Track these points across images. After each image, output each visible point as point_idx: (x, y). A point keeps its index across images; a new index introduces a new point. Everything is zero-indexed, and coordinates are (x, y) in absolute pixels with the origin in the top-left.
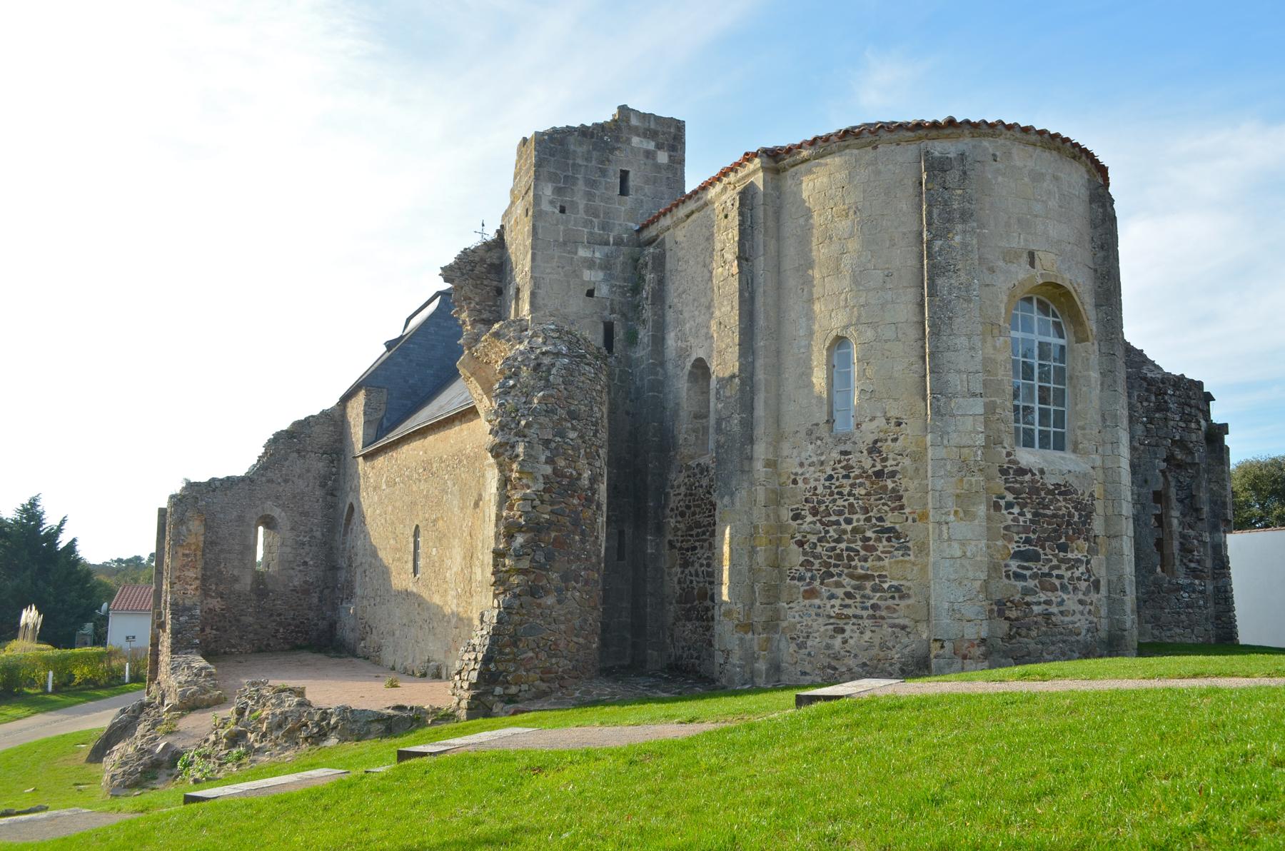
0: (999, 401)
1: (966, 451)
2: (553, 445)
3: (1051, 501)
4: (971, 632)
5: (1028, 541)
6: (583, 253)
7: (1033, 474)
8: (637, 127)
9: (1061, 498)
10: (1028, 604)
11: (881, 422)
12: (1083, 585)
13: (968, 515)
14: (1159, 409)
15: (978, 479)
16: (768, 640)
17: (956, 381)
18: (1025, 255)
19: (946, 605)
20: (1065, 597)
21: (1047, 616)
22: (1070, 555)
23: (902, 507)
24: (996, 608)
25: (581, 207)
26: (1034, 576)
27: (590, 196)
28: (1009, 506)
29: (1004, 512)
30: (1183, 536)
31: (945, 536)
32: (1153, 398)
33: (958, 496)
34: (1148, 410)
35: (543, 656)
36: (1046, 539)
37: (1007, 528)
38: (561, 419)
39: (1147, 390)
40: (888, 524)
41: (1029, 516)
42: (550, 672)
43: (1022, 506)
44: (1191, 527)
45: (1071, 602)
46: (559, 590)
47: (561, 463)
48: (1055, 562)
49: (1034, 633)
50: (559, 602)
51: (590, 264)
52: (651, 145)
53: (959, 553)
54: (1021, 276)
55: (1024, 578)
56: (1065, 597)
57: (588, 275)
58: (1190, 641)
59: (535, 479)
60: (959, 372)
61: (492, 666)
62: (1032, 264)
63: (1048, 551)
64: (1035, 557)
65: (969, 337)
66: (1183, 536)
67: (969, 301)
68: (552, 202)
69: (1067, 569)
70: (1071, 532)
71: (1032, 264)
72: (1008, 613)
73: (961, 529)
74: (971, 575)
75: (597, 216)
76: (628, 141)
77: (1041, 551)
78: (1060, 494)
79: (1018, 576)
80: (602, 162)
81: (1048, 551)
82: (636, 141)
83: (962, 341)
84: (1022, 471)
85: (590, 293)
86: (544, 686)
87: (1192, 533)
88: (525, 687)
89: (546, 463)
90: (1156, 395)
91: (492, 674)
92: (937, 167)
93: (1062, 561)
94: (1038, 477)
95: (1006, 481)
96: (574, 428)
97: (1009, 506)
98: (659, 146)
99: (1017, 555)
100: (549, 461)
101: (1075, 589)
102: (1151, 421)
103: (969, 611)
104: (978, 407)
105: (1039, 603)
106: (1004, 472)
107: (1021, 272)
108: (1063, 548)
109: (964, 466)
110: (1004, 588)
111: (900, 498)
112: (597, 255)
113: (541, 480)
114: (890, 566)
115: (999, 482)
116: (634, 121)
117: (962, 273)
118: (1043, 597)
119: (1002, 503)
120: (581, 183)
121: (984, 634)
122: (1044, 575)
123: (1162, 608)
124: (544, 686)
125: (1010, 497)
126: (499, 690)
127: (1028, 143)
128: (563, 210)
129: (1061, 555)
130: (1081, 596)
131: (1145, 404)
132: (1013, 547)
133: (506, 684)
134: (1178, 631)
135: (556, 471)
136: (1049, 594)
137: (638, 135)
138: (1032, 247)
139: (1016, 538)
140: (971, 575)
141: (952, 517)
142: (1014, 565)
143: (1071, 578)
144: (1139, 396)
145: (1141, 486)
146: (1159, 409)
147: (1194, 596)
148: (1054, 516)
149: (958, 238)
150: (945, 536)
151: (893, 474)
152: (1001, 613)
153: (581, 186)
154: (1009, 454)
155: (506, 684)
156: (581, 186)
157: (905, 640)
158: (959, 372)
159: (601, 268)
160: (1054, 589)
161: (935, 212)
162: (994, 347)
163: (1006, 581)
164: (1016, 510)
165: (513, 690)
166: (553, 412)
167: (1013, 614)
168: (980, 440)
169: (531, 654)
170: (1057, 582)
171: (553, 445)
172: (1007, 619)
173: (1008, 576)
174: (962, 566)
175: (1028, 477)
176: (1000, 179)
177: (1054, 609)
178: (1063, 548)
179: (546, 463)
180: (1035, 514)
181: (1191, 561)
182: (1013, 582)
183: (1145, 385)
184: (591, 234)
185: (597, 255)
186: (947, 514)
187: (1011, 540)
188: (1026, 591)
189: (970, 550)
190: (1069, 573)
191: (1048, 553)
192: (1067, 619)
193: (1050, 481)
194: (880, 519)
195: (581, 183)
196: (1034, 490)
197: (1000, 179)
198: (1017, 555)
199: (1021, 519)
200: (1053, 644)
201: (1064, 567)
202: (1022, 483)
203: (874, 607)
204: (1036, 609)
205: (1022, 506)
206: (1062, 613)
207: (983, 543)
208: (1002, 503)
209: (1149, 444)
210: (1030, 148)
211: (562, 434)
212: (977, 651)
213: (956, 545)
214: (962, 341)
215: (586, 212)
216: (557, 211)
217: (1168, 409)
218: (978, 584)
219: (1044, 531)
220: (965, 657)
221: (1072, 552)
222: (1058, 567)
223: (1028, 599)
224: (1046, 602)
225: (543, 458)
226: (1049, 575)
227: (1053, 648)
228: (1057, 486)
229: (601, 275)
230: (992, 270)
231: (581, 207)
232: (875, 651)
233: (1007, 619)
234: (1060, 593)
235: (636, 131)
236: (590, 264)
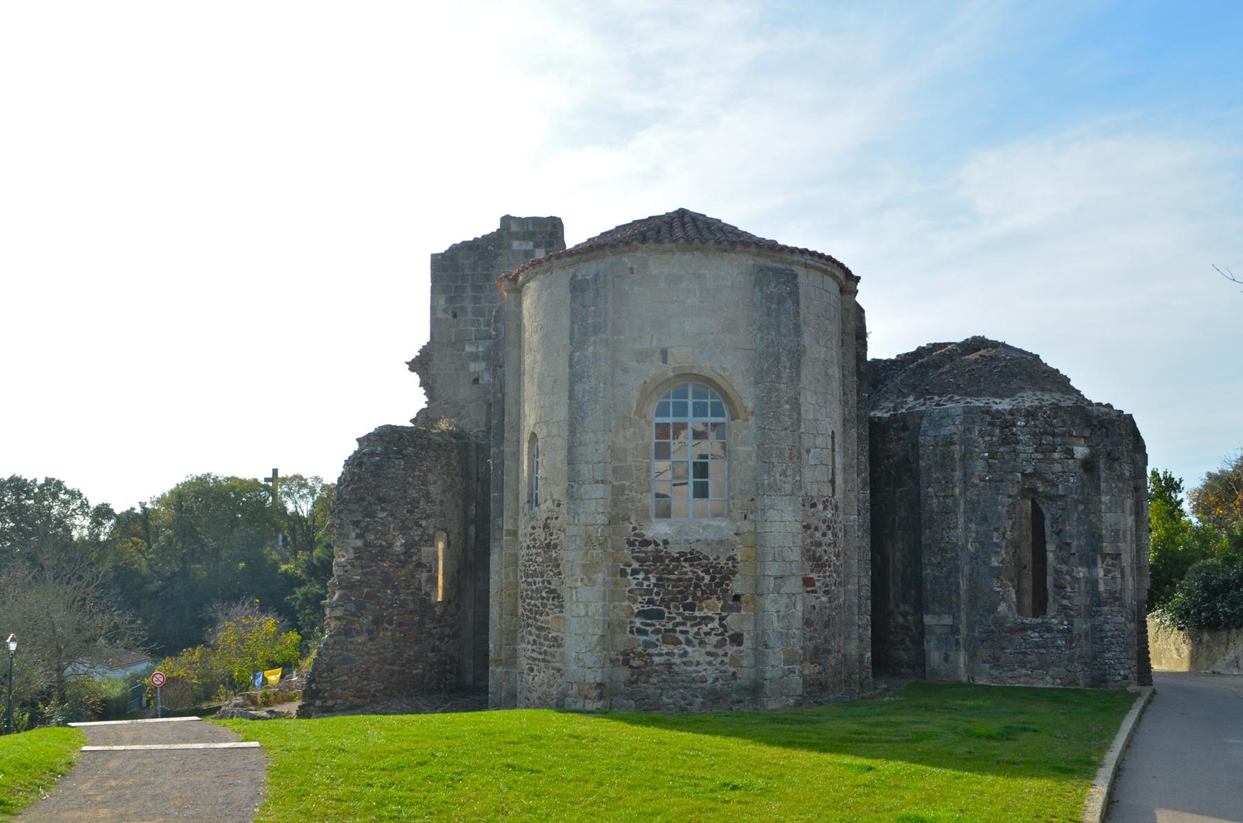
0: (627, 483)
1: (590, 528)
2: (363, 524)
3: (676, 568)
4: (594, 676)
5: (650, 602)
6: (469, 349)
7: (657, 544)
8: (516, 233)
9: (687, 564)
10: (650, 655)
11: (549, 503)
12: (713, 639)
13: (592, 582)
14: (1005, 441)
15: (598, 551)
16: (507, 673)
17: (585, 471)
18: (658, 355)
19: (574, 655)
20: (689, 649)
21: (669, 665)
22: (697, 614)
23: (560, 573)
24: (621, 658)
25: (469, 310)
26: (657, 632)
27: (476, 300)
28: (635, 572)
29: (630, 577)
30: (1056, 571)
31: (574, 598)
32: (997, 431)
33: (584, 566)
34: (991, 444)
35: (356, 679)
36: (671, 600)
37: (630, 591)
38: (370, 504)
39: (990, 424)
40: (553, 587)
41: (653, 580)
42: (362, 691)
43: (647, 572)
44: (1065, 562)
45: (695, 653)
46: (370, 632)
47: (371, 537)
48: (679, 619)
49: (654, 680)
50: (371, 639)
51: (475, 357)
52: (530, 246)
53: (583, 613)
54: (653, 372)
55: (645, 633)
56: (689, 649)
57: (473, 367)
58: (1040, 685)
59: (347, 551)
60: (587, 462)
61: (313, 686)
62: (665, 361)
63: (672, 609)
64: (660, 615)
65: (595, 433)
66: (1056, 571)
67: (596, 402)
68: (445, 311)
69: (692, 626)
70: (699, 594)
71: (665, 361)
72: (632, 663)
73: (586, 593)
74: (591, 631)
75: (482, 315)
76: (509, 246)
77: (666, 610)
78: (685, 561)
79: (640, 632)
80: (487, 269)
81: (672, 609)
82: (516, 245)
83: (590, 437)
84: (646, 543)
85: (476, 381)
86: (357, 701)
87: (1065, 568)
88: (339, 701)
89: (357, 538)
90: (1002, 429)
91: (313, 691)
92: (577, 287)
93: (686, 618)
94: (661, 547)
95: (633, 551)
96: (383, 510)
97: (635, 572)
98: (537, 246)
99: (641, 614)
100: (359, 536)
101: (702, 643)
102: (992, 456)
103: (589, 660)
104: (600, 491)
105: (661, 655)
106: (631, 544)
107: (653, 369)
108: (691, 607)
109: (589, 541)
110: (624, 640)
111: (558, 566)
112: (481, 349)
113: (351, 551)
114: (548, 619)
115: (627, 552)
116: (514, 228)
117: (593, 379)
118: (665, 649)
119: (629, 570)
120: (469, 290)
121: (599, 680)
122: (667, 631)
123: (1002, 649)
124: (357, 701)
125: (636, 565)
126: (318, 703)
127: (664, 252)
128: (455, 316)
129: (687, 613)
130: (709, 648)
131: (987, 439)
132: (636, 608)
133: (324, 699)
134: (1024, 671)
135: (367, 544)
136: (671, 647)
137: (518, 239)
138: (665, 345)
139: (640, 599)
140: (591, 631)
141: (579, 583)
142: (638, 622)
143: (698, 633)
144: (980, 431)
145: (981, 524)
146: (1005, 441)
147: (1047, 635)
148: (679, 580)
149: (591, 349)
150: (574, 598)
151: (555, 546)
152: (626, 663)
153: (469, 292)
154: (634, 529)
155: (324, 699)
156: (469, 292)
157: (559, 680)
158: (587, 462)
159: (483, 359)
160: (677, 642)
161: (576, 327)
162: (625, 438)
163: (630, 636)
164: (641, 576)
165: (330, 703)
166: (362, 499)
167: (636, 663)
168: (602, 519)
169: (345, 678)
170: (682, 638)
171: (363, 524)
172: (631, 667)
173: (631, 632)
174: (585, 623)
175: (651, 548)
176: (636, 289)
177: (677, 660)
178: (691, 607)
179: (357, 538)
180: (659, 579)
181: (1064, 597)
182: (636, 636)
183: (988, 418)
184: (477, 331)
185: (481, 349)
186: (576, 580)
187: (635, 601)
188: (647, 644)
189: (591, 610)
190: (696, 629)
191: (674, 613)
192: (690, 669)
193: (674, 550)
194: (549, 583)
195: (469, 290)
196: (658, 558)
197: (636, 289)
198: (641, 614)
199: (646, 583)
200: (674, 689)
201: (689, 624)
202: (646, 553)
203: (545, 652)
204: (657, 659)
205: (647, 572)
206: (684, 663)
207: (600, 605)
208: (629, 570)
209: (990, 480)
210: (668, 255)
211: (372, 515)
212: (595, 693)
213: (581, 606)
214: (590, 437)
215: (474, 314)
216: (449, 317)
217: (1018, 442)
218: (596, 638)
219: (668, 593)
220: (586, 698)
221: (701, 609)
222: (684, 624)
223: (650, 651)
224: (667, 654)
225: (353, 535)
226: (673, 631)
227: (672, 693)
228: (682, 554)
229: (483, 365)
230: (625, 371)
231: (469, 310)
232: (545, 688)
233: (631, 667)
234: (684, 646)
235: (515, 236)
236: (475, 357)
